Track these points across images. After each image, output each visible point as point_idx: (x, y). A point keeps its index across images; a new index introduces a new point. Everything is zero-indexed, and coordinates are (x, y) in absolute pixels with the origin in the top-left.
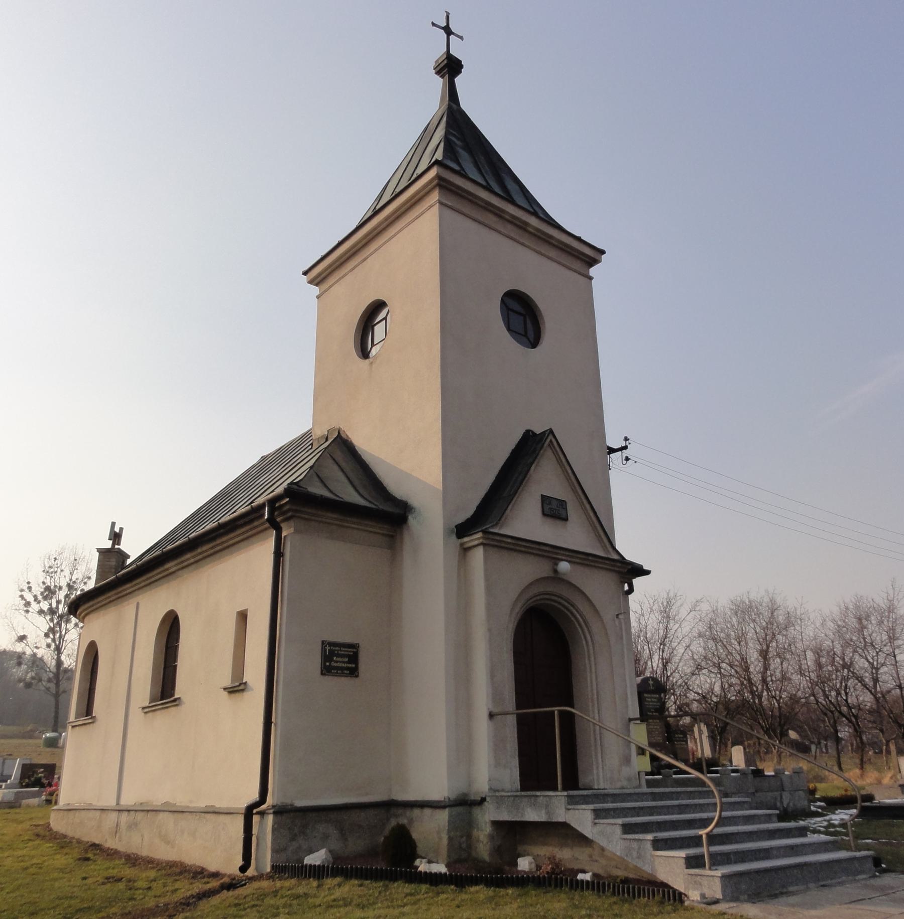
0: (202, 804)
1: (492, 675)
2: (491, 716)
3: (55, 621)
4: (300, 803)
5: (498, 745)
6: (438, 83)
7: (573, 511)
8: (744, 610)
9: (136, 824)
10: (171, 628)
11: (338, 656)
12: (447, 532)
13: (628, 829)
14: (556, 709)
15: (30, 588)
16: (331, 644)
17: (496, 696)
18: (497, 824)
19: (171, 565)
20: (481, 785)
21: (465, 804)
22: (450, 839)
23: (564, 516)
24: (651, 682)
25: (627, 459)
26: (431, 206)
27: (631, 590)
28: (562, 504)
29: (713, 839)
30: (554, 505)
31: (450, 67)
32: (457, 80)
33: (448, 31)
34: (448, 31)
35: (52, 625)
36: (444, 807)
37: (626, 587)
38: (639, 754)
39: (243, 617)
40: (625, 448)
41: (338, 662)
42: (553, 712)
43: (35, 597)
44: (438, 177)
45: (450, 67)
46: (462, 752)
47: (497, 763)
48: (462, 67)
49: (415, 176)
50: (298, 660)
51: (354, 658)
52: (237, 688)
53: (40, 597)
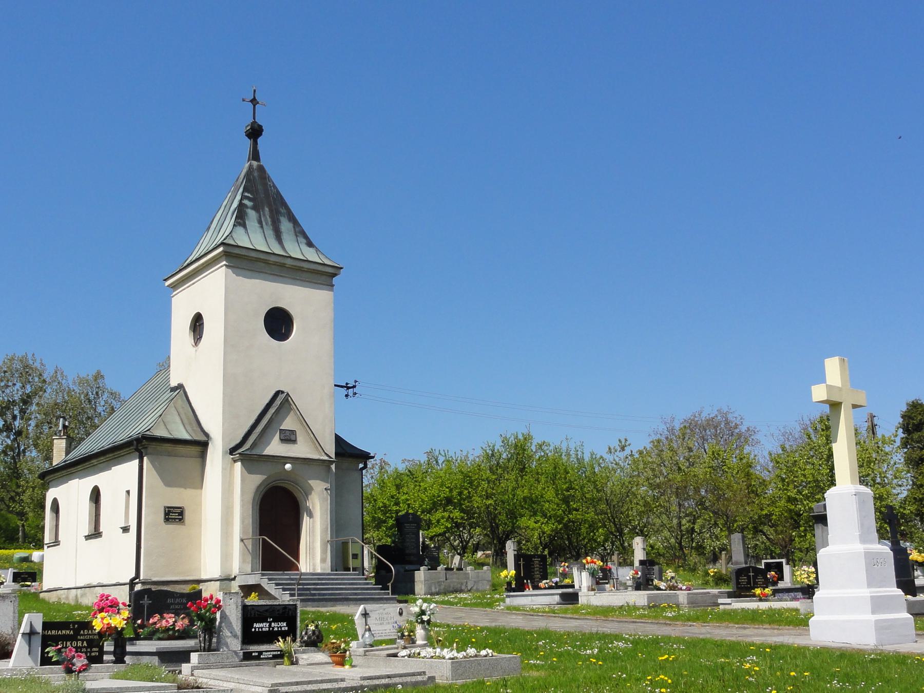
0: (114, 582)
2: (242, 540)
4: (155, 579)
5: (242, 555)
6: (248, 142)
7: (300, 438)
8: (691, 428)
10: (96, 495)
12: (224, 453)
13: (277, 584)
17: (243, 530)
19: (94, 461)
20: (235, 571)
21: (227, 579)
25: (355, 394)
27: (365, 467)
28: (293, 432)
29: (299, 589)
30: (288, 433)
31: (255, 132)
32: (260, 140)
33: (254, 101)
34: (254, 101)
35: (9, 442)
39: (128, 492)
41: (172, 516)
45: (255, 132)
46: (226, 557)
47: (243, 561)
48: (261, 134)
50: (153, 515)
51: (181, 513)
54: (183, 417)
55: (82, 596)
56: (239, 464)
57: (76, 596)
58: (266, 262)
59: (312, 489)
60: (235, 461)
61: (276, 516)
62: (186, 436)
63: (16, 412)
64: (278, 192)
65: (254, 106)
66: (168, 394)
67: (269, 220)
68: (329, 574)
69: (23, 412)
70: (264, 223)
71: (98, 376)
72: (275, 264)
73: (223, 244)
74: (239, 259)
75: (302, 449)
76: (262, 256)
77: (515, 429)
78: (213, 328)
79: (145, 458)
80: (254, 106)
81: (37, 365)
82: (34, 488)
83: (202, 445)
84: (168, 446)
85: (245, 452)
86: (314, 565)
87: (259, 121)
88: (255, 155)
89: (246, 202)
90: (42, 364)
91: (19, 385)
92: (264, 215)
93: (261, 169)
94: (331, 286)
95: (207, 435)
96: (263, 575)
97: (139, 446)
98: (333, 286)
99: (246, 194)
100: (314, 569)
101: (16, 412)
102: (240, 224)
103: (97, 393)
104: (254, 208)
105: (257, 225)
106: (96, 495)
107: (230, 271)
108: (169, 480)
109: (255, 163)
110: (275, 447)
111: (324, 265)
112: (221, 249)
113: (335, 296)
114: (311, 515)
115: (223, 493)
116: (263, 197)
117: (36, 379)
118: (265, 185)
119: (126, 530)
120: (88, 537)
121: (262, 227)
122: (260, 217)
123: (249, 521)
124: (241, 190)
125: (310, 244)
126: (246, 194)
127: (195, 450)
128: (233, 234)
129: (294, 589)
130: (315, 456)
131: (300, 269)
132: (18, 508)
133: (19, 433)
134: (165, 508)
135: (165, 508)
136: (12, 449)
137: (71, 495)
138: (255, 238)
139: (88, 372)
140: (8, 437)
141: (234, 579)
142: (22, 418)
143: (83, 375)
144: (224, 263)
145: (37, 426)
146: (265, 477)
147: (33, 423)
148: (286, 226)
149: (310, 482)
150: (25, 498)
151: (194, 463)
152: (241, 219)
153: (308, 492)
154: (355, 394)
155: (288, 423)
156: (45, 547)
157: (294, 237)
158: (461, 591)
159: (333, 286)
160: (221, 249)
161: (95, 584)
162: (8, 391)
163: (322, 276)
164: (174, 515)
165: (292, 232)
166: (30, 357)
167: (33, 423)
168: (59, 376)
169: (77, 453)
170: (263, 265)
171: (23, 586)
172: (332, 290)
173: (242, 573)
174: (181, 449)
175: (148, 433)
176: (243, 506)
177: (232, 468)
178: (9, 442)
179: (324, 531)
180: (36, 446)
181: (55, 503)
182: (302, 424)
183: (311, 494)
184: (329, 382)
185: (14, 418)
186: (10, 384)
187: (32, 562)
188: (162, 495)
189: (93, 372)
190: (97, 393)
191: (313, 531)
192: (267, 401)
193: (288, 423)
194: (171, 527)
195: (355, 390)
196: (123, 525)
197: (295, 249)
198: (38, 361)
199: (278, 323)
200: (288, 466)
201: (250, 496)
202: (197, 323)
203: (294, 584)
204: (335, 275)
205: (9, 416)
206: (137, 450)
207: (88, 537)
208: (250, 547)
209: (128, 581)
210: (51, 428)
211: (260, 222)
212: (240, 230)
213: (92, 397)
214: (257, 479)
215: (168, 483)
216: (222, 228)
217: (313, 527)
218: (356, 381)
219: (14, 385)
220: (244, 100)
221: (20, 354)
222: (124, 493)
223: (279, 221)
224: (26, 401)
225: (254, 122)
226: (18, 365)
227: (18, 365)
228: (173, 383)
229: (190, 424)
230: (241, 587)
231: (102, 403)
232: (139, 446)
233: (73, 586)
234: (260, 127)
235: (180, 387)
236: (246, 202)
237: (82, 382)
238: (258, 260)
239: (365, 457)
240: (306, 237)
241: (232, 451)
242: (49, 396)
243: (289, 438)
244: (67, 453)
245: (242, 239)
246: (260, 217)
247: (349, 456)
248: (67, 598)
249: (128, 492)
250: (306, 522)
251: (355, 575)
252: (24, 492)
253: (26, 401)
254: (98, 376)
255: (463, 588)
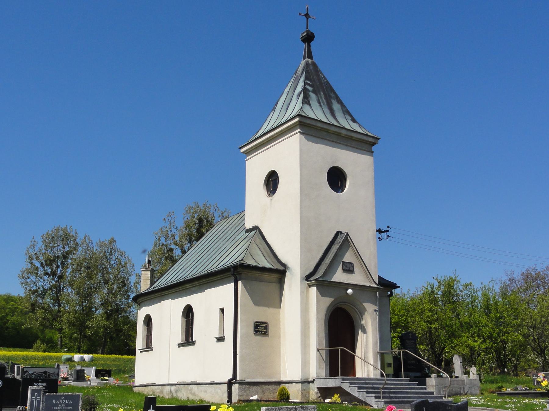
0: (209, 381)
1: (318, 335)
2: (318, 350)
3: (56, 279)
4: (248, 380)
5: (319, 363)
6: (303, 46)
7: (357, 269)
9: (180, 390)
10: (188, 312)
11: (260, 326)
12: (302, 280)
13: (359, 388)
14: (339, 348)
15: (37, 258)
16: (257, 322)
17: (319, 342)
18: (319, 389)
19: (188, 286)
20: (313, 373)
21: (306, 382)
22: (302, 393)
23: (352, 270)
24: (410, 335)
25: (388, 236)
26: (296, 133)
28: (352, 264)
29: (383, 393)
30: (348, 265)
32: (312, 44)
33: (307, 16)
34: (307, 16)
36: (300, 383)
37: (389, 293)
38: (388, 367)
39: (222, 310)
40: (388, 231)
41: (260, 329)
42: (338, 350)
43: (42, 264)
44: (299, 121)
45: (308, 38)
46: (305, 363)
47: (319, 367)
48: (313, 40)
49: (289, 118)
51: (266, 327)
52: (220, 339)
53: (44, 264)
54: (263, 251)
55: (176, 391)
56: (314, 288)
57: (171, 391)
58: (327, 131)
59: (365, 310)
60: (310, 286)
61: (340, 330)
62: (269, 266)
63: (59, 264)
64: (327, 82)
65: (307, 19)
66: (243, 235)
67: (325, 101)
68: (378, 380)
69: (62, 263)
70: (322, 104)
71: (112, 241)
72: (334, 133)
73: (299, 115)
74: (309, 128)
75: (357, 278)
76: (325, 126)
77: (444, 273)
78: (289, 184)
79: (240, 283)
80: (307, 19)
81: (73, 233)
82: (69, 313)
83: (280, 273)
84: (256, 273)
85: (318, 278)
86: (368, 372)
87: (311, 29)
88: (310, 56)
89: (308, 87)
90: (76, 233)
91: (61, 246)
92: (321, 98)
93: (314, 64)
94: (371, 152)
95: (284, 265)
96: (343, 379)
97: (236, 272)
98: (373, 152)
99: (307, 82)
100: (368, 375)
101: (59, 264)
102: (306, 103)
103: (111, 251)
104: (314, 92)
105: (318, 104)
106: (188, 312)
107: (303, 137)
108: (258, 300)
109: (310, 60)
110: (339, 276)
111: (367, 135)
112: (297, 119)
113: (374, 159)
114: (364, 331)
115: (302, 312)
116: (318, 86)
117: (72, 242)
118: (318, 76)
119: (220, 339)
120: (180, 345)
121: (321, 106)
122: (318, 99)
123: (323, 334)
124: (302, 79)
125: (354, 121)
126: (307, 82)
127: (274, 277)
128: (303, 109)
129: (379, 393)
130: (368, 284)
131: (351, 138)
132: (58, 325)
133: (61, 277)
134: (255, 322)
135: (255, 322)
136: (56, 288)
137: (166, 314)
138: (317, 112)
139: (106, 238)
140: (53, 279)
141: (313, 382)
142: (62, 268)
143: (103, 240)
144: (299, 130)
145: (73, 272)
146: (332, 299)
147: (69, 270)
148: (336, 106)
149: (365, 304)
150: (64, 319)
151: (274, 287)
152: (306, 100)
153: (362, 312)
154: (388, 236)
155: (348, 257)
156: (137, 352)
157: (343, 115)
158: (460, 394)
159: (373, 152)
160: (297, 119)
161: (188, 381)
162: (54, 250)
163: (364, 144)
164: (261, 329)
165: (341, 111)
166: (69, 228)
167: (69, 270)
168: (87, 241)
169: (161, 283)
170: (325, 133)
171: (102, 380)
172: (372, 156)
173: (319, 378)
174: (265, 276)
175: (242, 262)
176: (318, 322)
177: (308, 292)
178: (54, 282)
179: (375, 344)
180: (71, 285)
181: (148, 321)
182: (357, 258)
183: (364, 314)
184: (374, 228)
185: (58, 267)
186: (56, 245)
187: (73, 361)
188: (251, 313)
189: (108, 238)
190: (111, 251)
191: (367, 345)
192: (330, 239)
193: (348, 257)
194: (259, 338)
195: (388, 234)
196: (218, 336)
197: (345, 123)
198: (74, 231)
199: (336, 178)
200: (350, 291)
201: (323, 314)
202: (272, 181)
203: (378, 388)
204: (374, 144)
205: (54, 266)
206: (233, 275)
207: (180, 345)
208: (324, 356)
209: (226, 381)
210: (81, 274)
211: (319, 102)
212: (306, 107)
213: (107, 254)
214: (328, 301)
215: (257, 303)
216: (296, 106)
217: (367, 341)
218: (388, 227)
219: (59, 246)
220: (300, 14)
221: (63, 226)
222: (218, 311)
223: (332, 103)
224: (65, 256)
225: (308, 31)
226: (61, 233)
227: (61, 233)
228: (248, 226)
229: (269, 256)
230: (319, 389)
231: (114, 258)
232: (236, 272)
233: (167, 383)
234: (313, 34)
235: (256, 228)
236: (308, 87)
237: (102, 244)
238: (322, 129)
239: (394, 286)
240: (350, 115)
241: (308, 278)
242: (80, 253)
243: (349, 269)
244: (152, 283)
245: (309, 112)
246: (318, 99)
247: (387, 286)
248: (161, 392)
249: (222, 310)
250: (360, 337)
251: (407, 381)
252: (63, 315)
253: (65, 256)
254: (112, 241)
255: (462, 392)
